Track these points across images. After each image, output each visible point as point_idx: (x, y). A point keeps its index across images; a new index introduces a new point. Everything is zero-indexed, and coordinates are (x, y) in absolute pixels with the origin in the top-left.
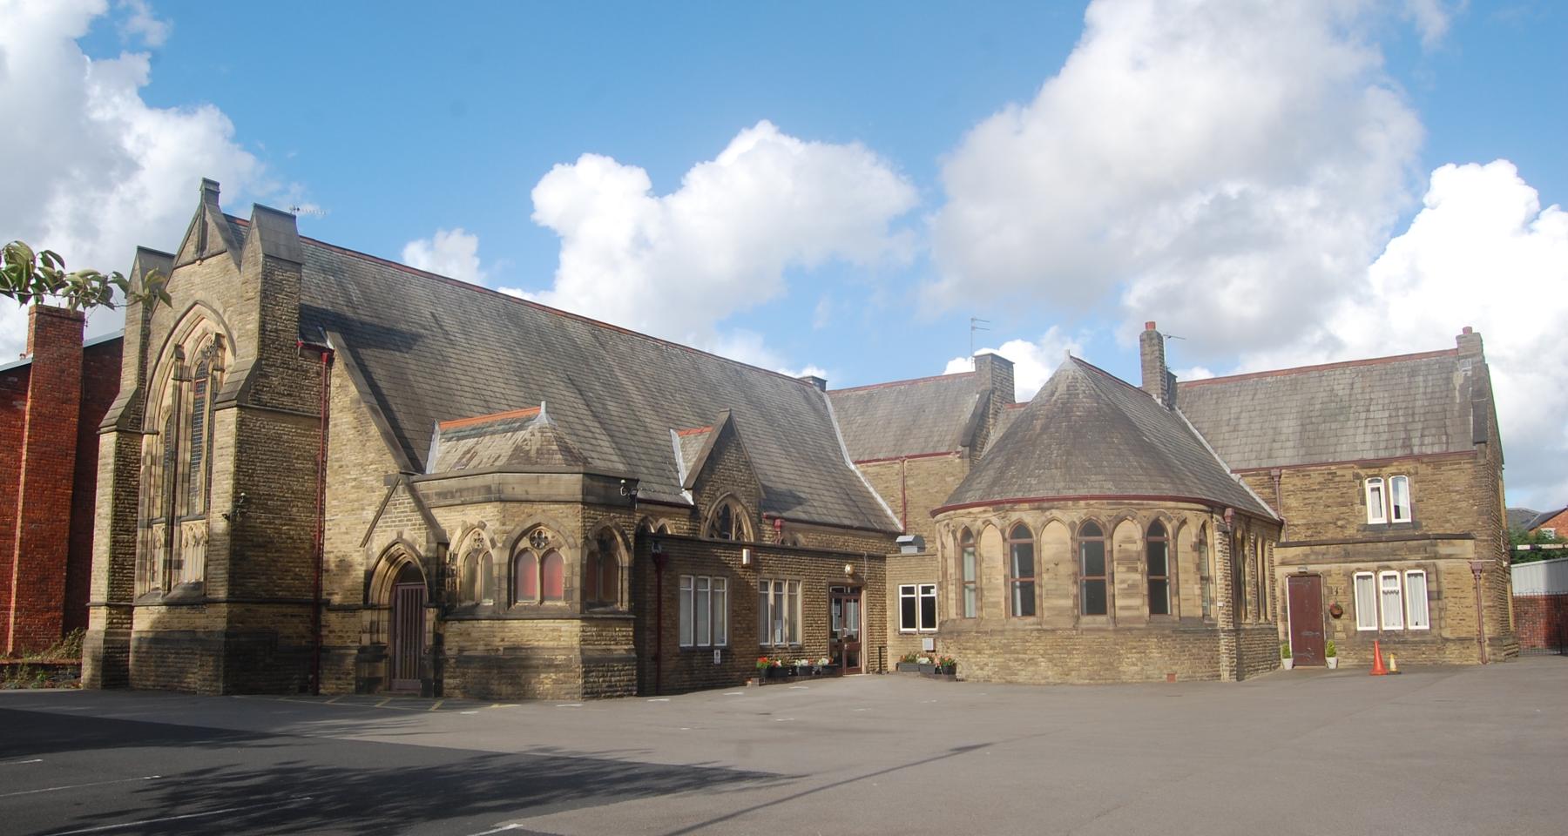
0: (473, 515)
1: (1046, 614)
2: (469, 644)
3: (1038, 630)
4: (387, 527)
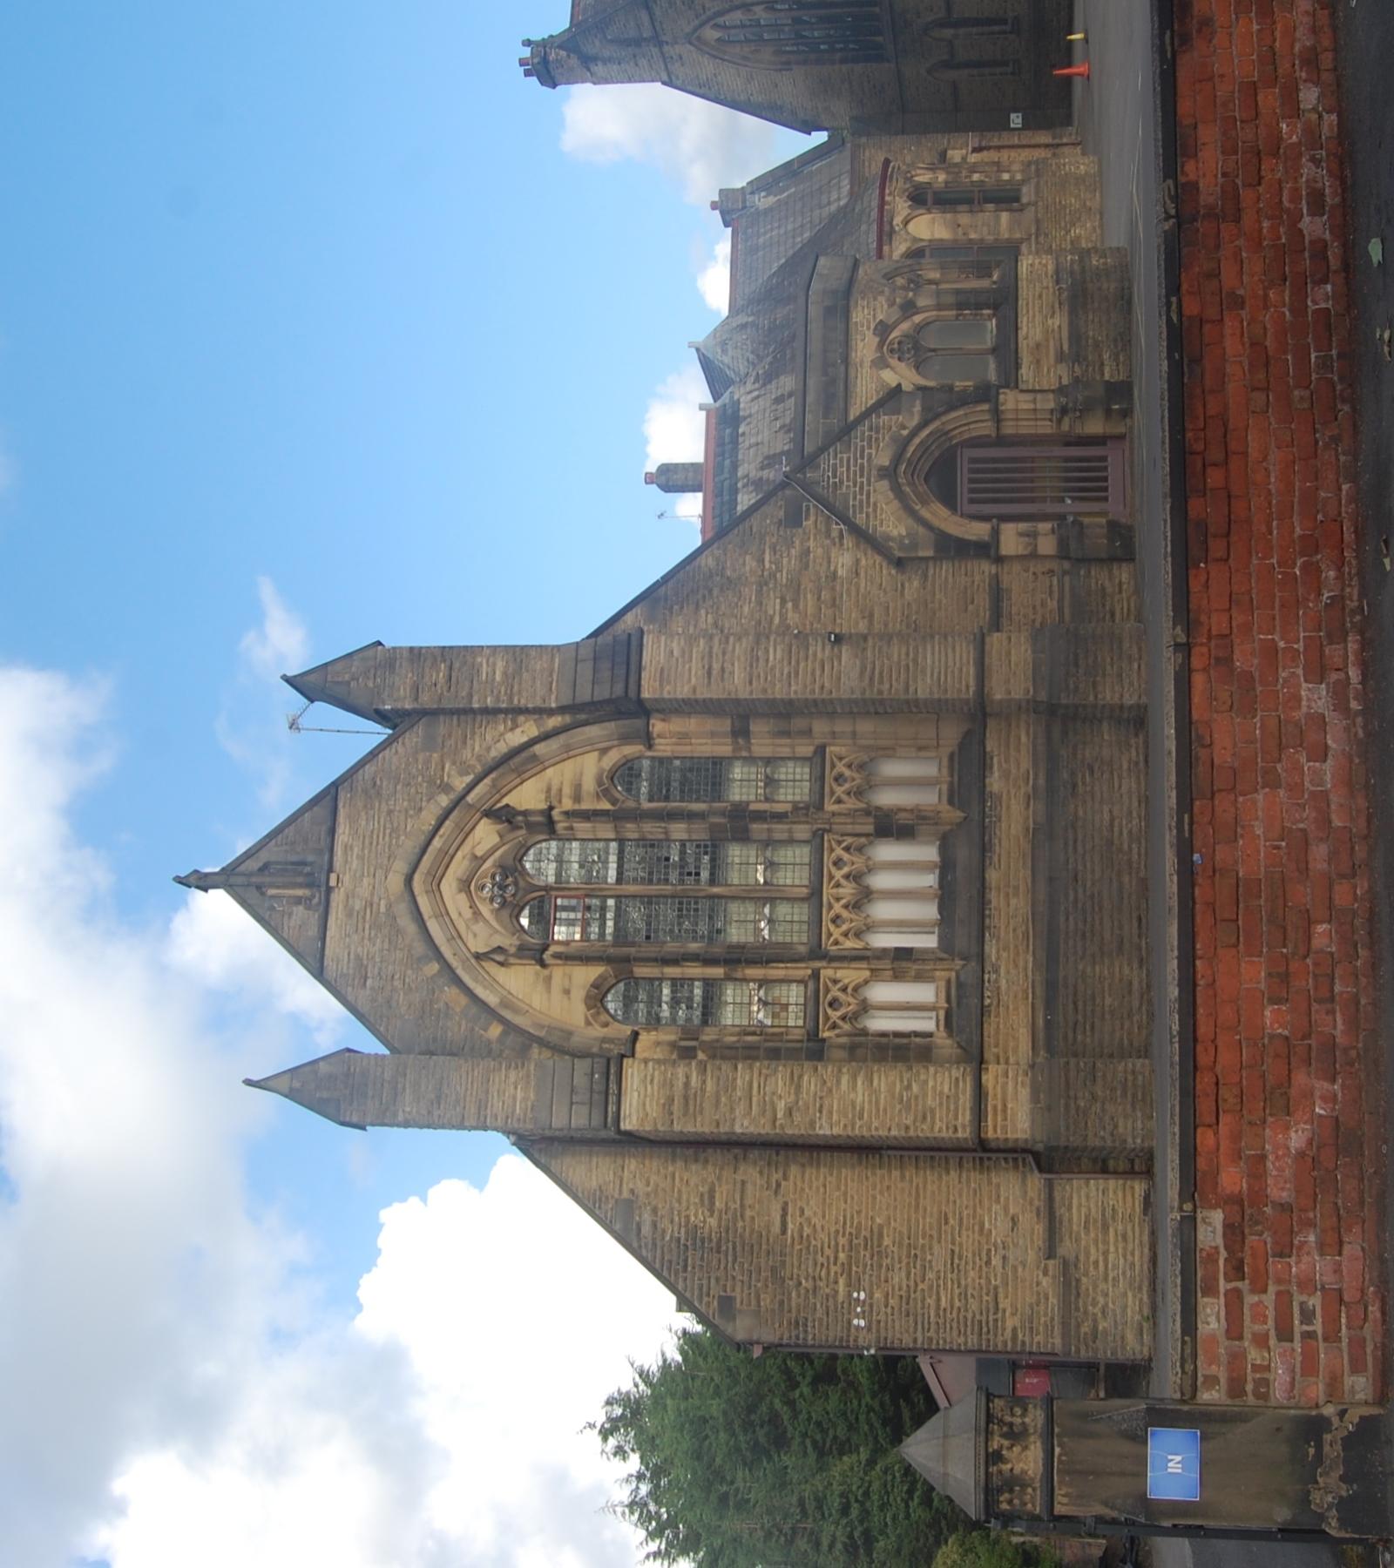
0: (865, 347)
1: (1018, 236)
2: (1052, 343)
3: (1037, 237)
4: (868, 503)
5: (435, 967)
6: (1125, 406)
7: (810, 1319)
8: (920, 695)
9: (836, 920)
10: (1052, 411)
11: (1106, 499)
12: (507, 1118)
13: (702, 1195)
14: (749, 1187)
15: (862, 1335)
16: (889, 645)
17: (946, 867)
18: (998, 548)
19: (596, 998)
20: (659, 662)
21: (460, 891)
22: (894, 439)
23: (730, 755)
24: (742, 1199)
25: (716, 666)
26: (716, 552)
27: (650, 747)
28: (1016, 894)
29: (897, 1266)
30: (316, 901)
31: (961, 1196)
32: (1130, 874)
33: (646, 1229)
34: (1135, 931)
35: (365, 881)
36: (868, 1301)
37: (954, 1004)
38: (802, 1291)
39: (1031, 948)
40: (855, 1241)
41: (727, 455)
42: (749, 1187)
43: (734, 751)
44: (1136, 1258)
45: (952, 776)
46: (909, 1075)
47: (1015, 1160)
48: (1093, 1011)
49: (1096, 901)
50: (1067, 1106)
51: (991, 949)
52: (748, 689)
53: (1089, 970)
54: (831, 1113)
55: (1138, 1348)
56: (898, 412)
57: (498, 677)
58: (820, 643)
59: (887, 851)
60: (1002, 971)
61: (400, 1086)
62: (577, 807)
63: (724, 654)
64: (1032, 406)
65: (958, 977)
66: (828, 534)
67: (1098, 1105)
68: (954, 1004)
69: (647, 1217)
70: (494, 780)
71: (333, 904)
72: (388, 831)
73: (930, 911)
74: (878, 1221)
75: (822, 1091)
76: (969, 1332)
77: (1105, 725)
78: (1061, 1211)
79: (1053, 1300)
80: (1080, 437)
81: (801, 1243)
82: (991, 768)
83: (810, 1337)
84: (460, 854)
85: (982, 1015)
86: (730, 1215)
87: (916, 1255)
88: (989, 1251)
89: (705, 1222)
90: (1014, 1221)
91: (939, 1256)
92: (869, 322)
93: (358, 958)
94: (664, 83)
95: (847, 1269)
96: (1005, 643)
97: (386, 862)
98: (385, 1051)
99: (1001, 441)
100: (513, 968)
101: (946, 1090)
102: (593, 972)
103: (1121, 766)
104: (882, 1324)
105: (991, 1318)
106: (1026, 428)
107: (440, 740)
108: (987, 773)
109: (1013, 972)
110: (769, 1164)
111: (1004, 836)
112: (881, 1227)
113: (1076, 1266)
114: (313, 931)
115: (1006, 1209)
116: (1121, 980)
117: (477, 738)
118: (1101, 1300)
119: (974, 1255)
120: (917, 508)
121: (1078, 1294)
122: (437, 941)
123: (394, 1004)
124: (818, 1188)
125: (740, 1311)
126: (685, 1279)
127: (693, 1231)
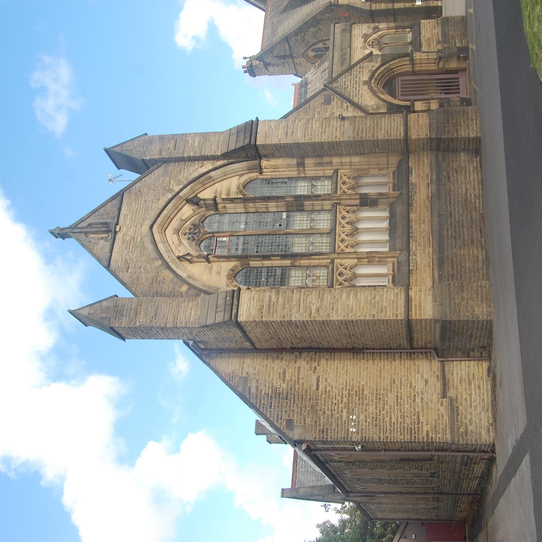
2: (434, 38)
4: (359, 94)
5: (160, 262)
6: (465, 55)
7: (329, 429)
8: (379, 138)
9: (342, 241)
10: (435, 59)
11: (459, 93)
12: (187, 323)
13: (280, 373)
14: (302, 369)
15: (354, 435)
16: (366, 120)
17: (392, 218)
18: (414, 108)
19: (233, 275)
20: (265, 131)
21: (174, 234)
22: (369, 71)
23: (296, 176)
24: (298, 375)
25: (290, 131)
26: (295, 115)
27: (261, 173)
28: (424, 223)
29: (371, 403)
30: (109, 238)
31: (401, 371)
32: (476, 212)
33: (253, 390)
34: (479, 235)
35: (132, 229)
36: (357, 420)
37: (396, 272)
38: (326, 416)
39: (431, 244)
40: (351, 392)
41: (302, 98)
42: (302, 369)
43: (298, 174)
44: (485, 397)
45: (394, 179)
46: (374, 293)
47: (426, 353)
48: (461, 269)
49: (460, 223)
50: (450, 303)
51: (413, 246)
52: (303, 139)
53: (458, 252)
54: (337, 310)
55: (488, 438)
56: (372, 62)
57: (196, 145)
58: (335, 121)
59: (366, 213)
60: (418, 255)
61: (139, 311)
62: (228, 197)
63: (293, 126)
64: (427, 57)
65: (398, 260)
66: (342, 106)
67: (465, 301)
68: (396, 272)
69: (254, 384)
70: (191, 187)
71: (117, 239)
72: (144, 209)
73: (386, 237)
74: (362, 383)
75: (333, 301)
76: (406, 433)
77: (462, 154)
78: (448, 376)
79: (446, 418)
80: (447, 71)
81: (326, 394)
82: (412, 173)
83: (329, 437)
84: (175, 219)
85: (409, 274)
86: (292, 382)
87: (380, 398)
88: (415, 395)
89: (280, 385)
90: (426, 382)
91: (391, 398)
92: (360, 34)
93: (126, 260)
94: (294, 75)
95: (347, 406)
96: (417, 117)
97: (142, 221)
98: (131, 296)
99: (414, 73)
100: (195, 264)
101: (392, 298)
102: (231, 264)
103: (470, 170)
104: (364, 431)
105: (416, 427)
106: (425, 67)
107: (170, 172)
108: (410, 176)
109: (423, 255)
110: (311, 359)
111: (418, 200)
112: (363, 386)
113: (456, 401)
114: (107, 250)
115: (422, 376)
116: (473, 256)
117: (186, 171)
118: (469, 417)
119: (408, 397)
120: (379, 95)
121: (458, 414)
122: (162, 252)
123: (140, 278)
124: (334, 370)
125: (296, 426)
126: (271, 412)
127: (275, 390)
